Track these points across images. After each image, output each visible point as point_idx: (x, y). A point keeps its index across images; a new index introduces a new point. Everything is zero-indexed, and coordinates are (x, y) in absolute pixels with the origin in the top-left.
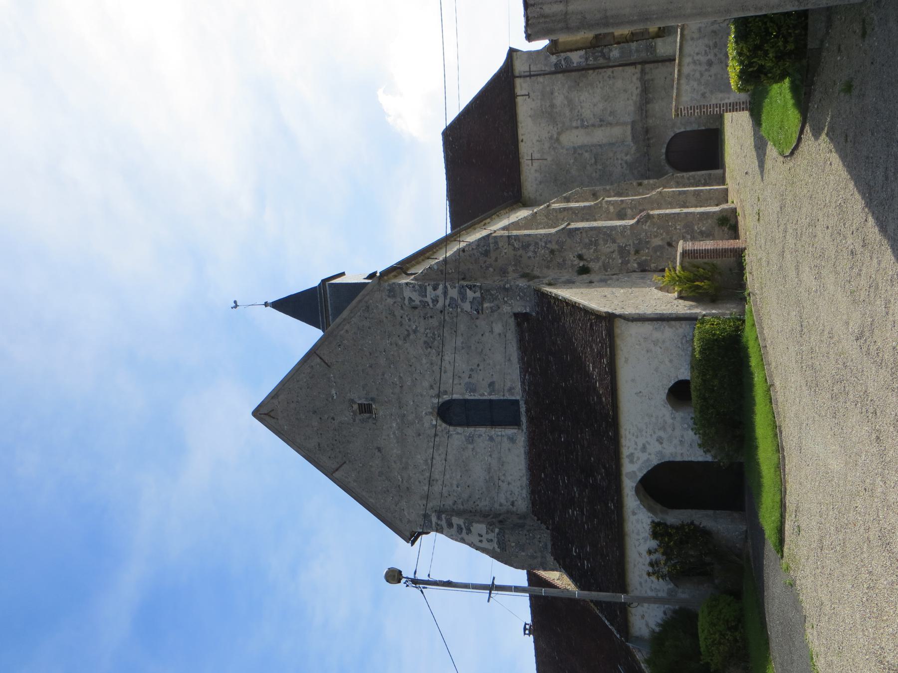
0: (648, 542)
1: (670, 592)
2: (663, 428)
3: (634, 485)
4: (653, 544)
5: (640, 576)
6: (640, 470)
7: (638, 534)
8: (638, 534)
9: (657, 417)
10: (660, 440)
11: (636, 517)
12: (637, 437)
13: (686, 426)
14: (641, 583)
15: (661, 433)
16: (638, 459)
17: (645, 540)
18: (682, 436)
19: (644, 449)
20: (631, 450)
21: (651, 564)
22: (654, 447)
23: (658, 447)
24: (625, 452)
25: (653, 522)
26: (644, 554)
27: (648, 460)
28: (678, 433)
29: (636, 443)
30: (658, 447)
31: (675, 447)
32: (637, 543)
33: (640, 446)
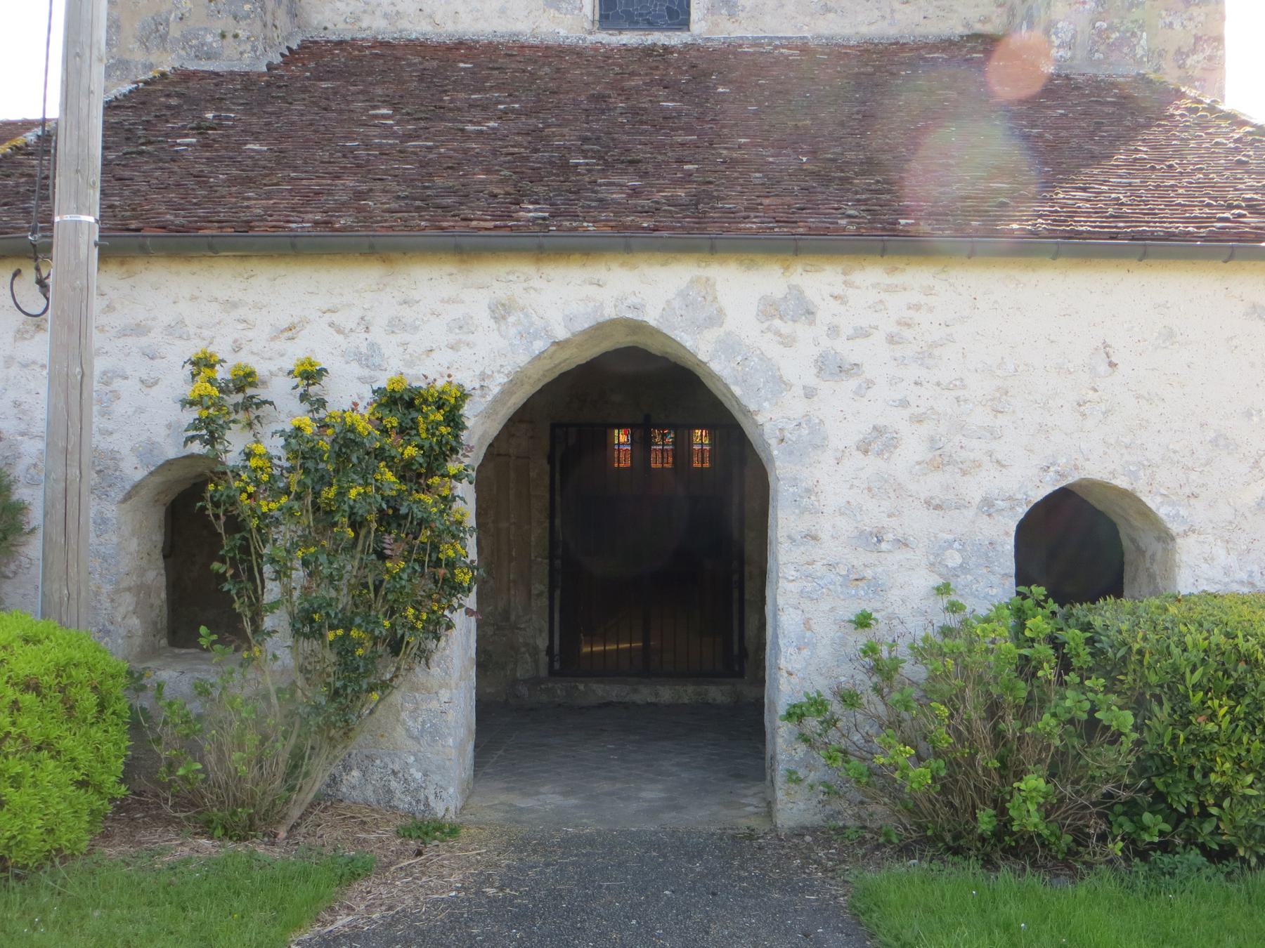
0: (356, 369)
1: (106, 468)
2: (939, 460)
3: (651, 317)
4: (350, 393)
5: (175, 329)
6: (729, 346)
7: (395, 325)
8: (395, 325)
9: (993, 434)
10: (878, 441)
11: (483, 317)
12: (892, 339)
13: (954, 559)
14: (139, 329)
15: (912, 448)
16: (787, 341)
17: (368, 358)
18: (902, 543)
19: (835, 368)
20: (827, 311)
21: (245, 380)
22: (844, 415)
23: (844, 434)
24: (820, 281)
25: (463, 396)
26: (294, 353)
27: (780, 384)
28: (918, 522)
29: (862, 333)
30: (844, 434)
31: (847, 510)
32: (348, 319)
33: (851, 351)
